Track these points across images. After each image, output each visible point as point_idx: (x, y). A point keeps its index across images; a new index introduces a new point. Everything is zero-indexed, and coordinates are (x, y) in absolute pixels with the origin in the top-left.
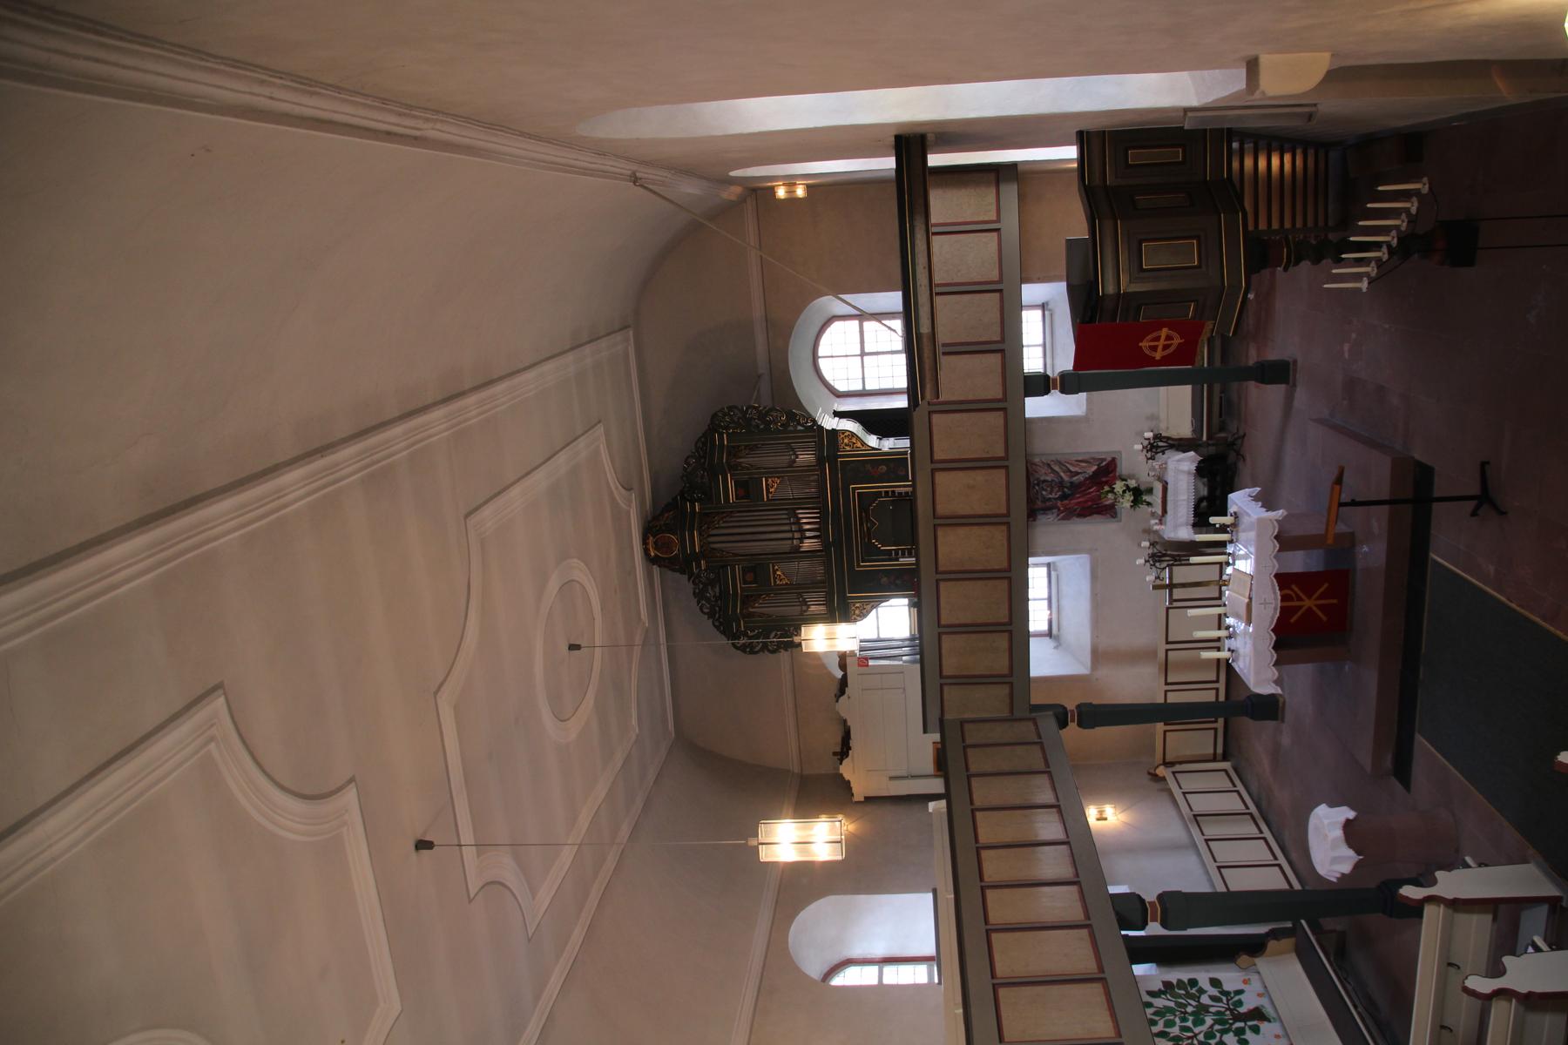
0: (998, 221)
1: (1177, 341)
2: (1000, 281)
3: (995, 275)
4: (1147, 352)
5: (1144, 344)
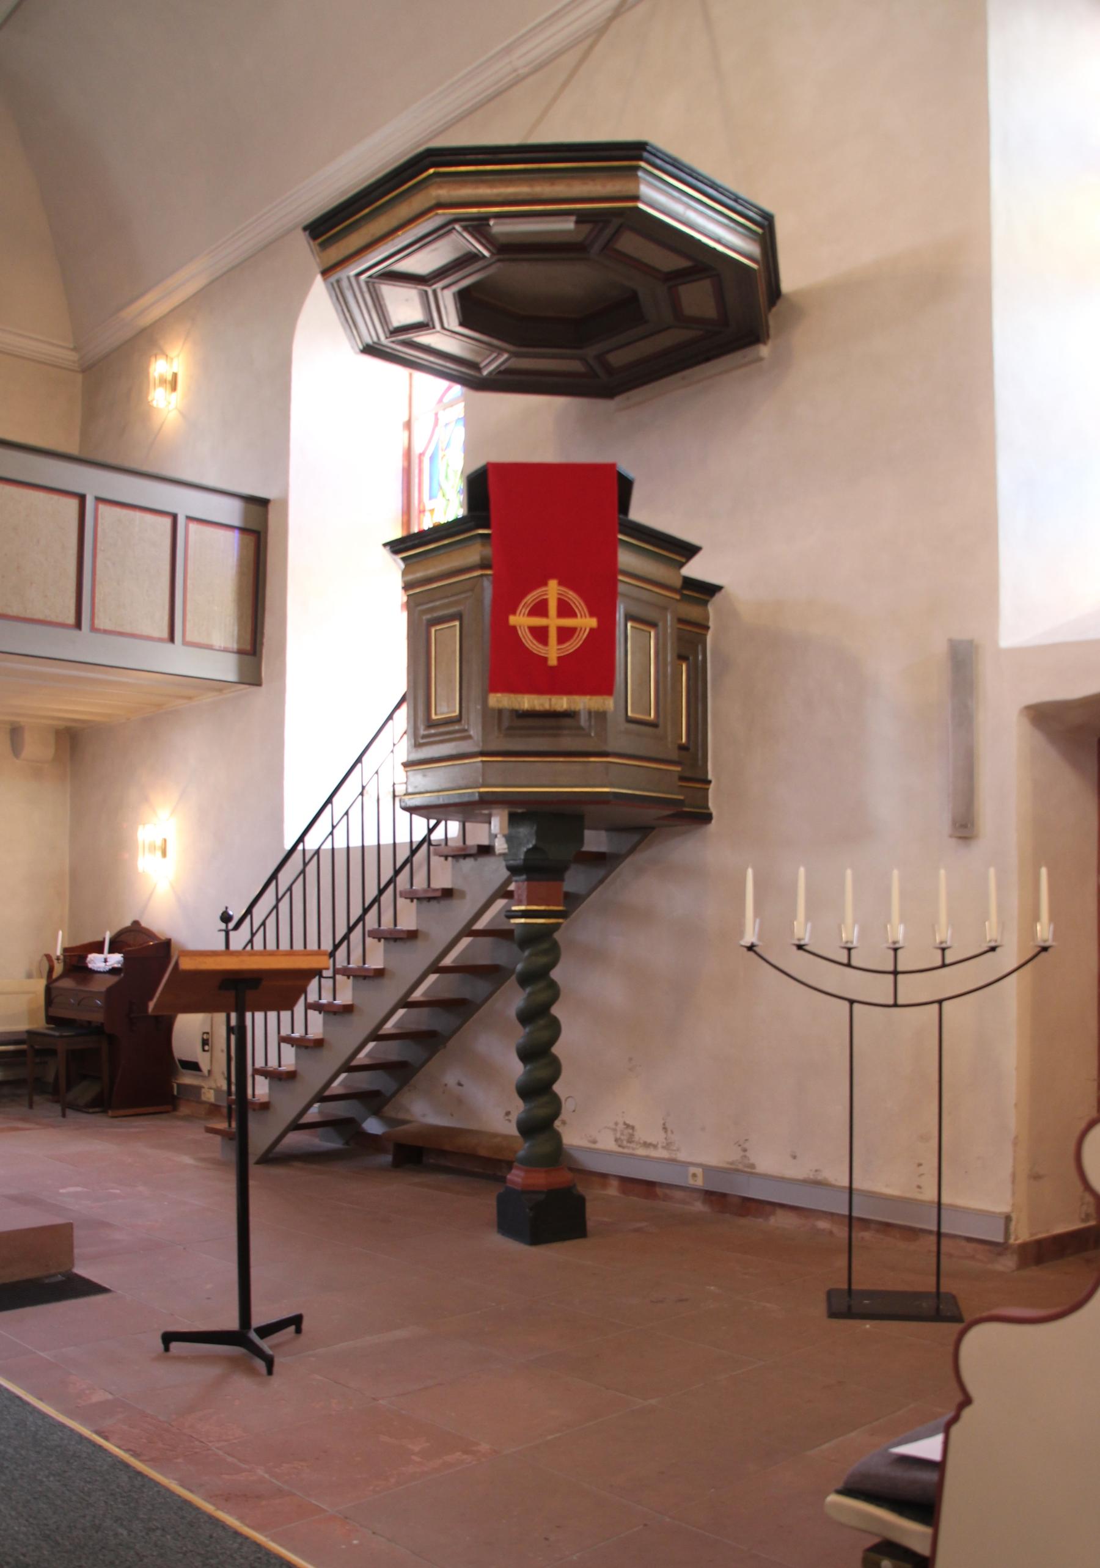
0: (185, 643)
1: (553, 653)
2: (93, 629)
3: (102, 622)
4: (531, 598)
5: (553, 590)
